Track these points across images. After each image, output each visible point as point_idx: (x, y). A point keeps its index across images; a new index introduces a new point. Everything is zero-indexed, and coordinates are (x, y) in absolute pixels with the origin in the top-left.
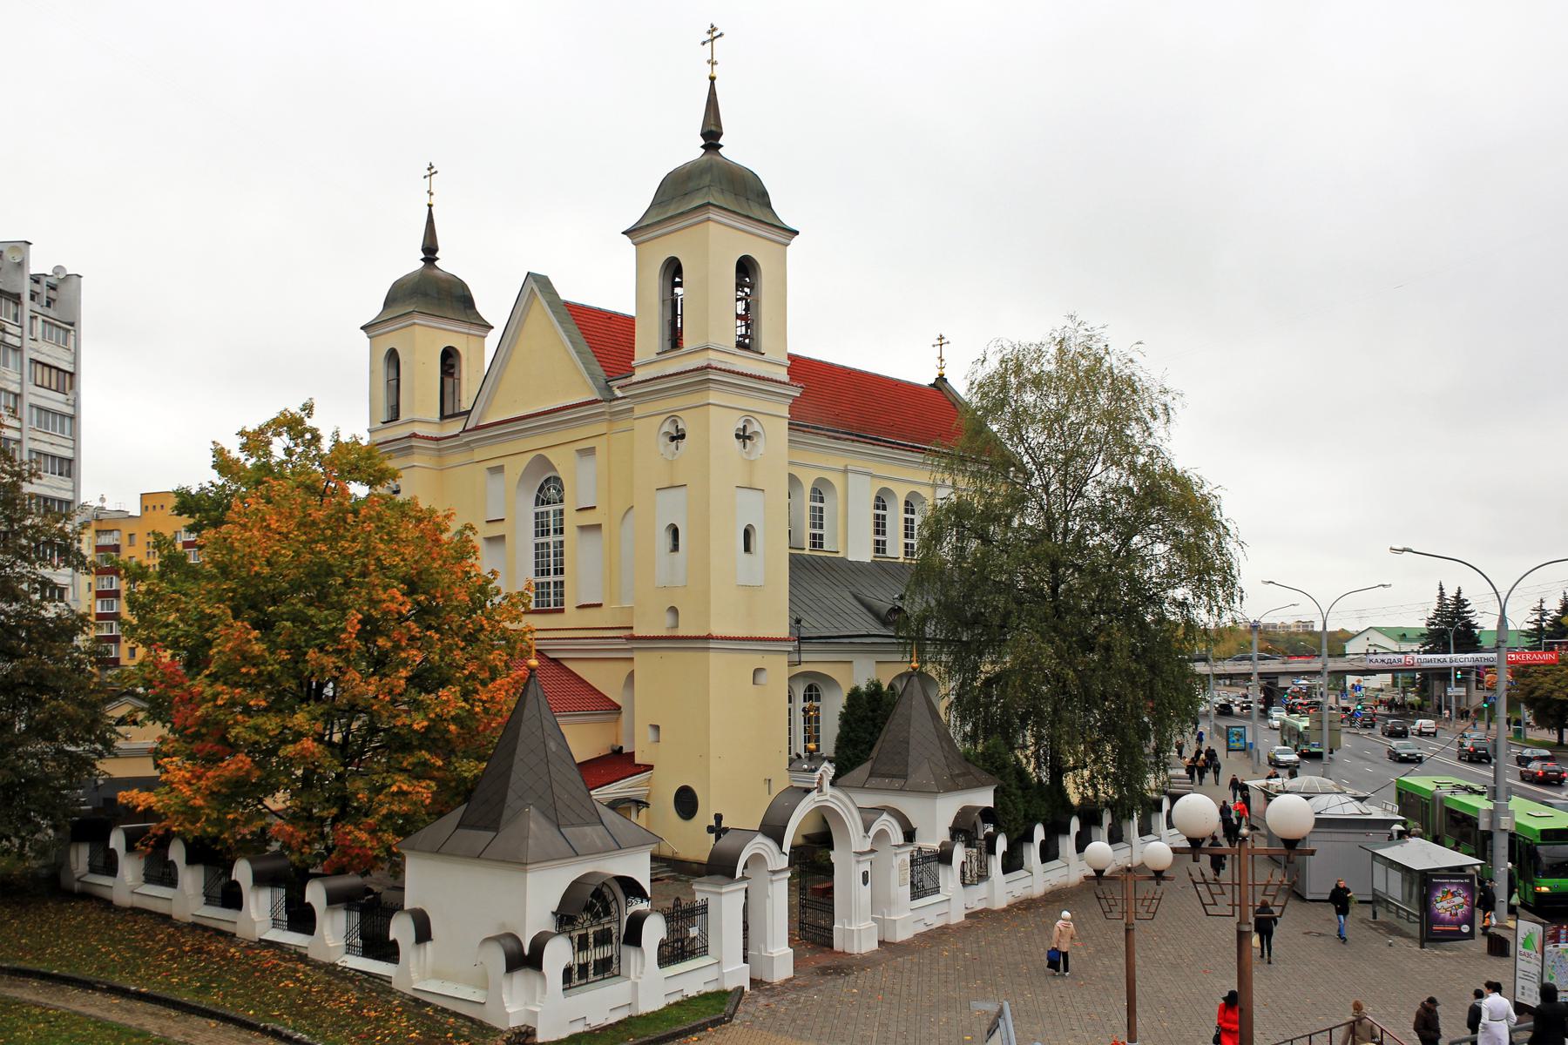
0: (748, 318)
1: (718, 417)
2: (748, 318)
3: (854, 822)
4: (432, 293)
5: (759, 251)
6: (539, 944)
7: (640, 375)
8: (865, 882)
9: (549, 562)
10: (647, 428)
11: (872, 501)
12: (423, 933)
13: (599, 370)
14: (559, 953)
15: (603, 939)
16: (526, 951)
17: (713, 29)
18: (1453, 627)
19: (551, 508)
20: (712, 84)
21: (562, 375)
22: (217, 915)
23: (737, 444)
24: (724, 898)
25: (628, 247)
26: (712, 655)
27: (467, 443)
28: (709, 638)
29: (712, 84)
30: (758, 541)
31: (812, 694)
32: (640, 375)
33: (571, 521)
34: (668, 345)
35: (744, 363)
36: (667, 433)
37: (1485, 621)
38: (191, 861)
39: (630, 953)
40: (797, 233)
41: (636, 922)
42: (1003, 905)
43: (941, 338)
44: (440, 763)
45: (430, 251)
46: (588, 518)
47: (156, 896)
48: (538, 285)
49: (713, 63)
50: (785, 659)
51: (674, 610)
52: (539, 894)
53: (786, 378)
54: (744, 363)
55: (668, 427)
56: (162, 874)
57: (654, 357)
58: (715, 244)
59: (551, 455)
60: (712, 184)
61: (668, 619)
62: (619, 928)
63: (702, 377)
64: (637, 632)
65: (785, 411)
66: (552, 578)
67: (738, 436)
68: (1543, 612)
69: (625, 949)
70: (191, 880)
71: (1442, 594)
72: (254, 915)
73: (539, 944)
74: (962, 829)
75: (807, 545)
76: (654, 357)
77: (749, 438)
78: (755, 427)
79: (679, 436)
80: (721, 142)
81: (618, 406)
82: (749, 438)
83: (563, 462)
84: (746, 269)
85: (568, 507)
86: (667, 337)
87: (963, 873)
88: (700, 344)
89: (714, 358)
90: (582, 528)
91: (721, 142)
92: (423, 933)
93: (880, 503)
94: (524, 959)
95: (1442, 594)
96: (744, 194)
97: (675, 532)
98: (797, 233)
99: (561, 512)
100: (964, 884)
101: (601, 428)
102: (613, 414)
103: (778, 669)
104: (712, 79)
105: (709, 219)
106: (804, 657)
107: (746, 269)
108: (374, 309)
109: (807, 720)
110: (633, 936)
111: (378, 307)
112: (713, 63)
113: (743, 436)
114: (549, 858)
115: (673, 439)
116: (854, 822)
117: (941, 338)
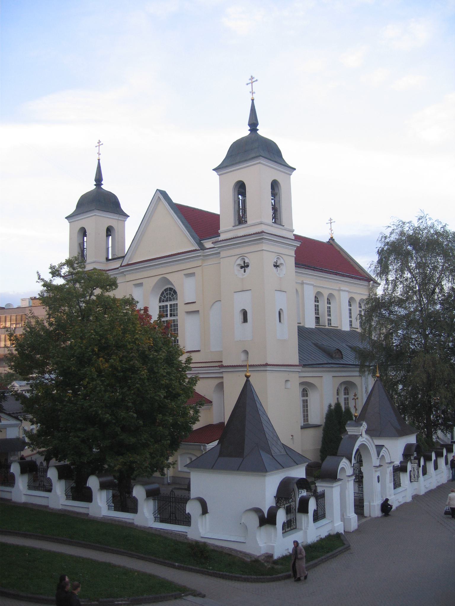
0: (275, 210)
1: (263, 257)
2: (275, 210)
4: (100, 201)
7: (222, 237)
8: (379, 482)
10: (229, 262)
11: (313, 299)
12: (205, 511)
13: (196, 236)
14: (281, 516)
16: (266, 516)
19: (168, 303)
20: (99, 163)
21: (181, 239)
22: (78, 506)
23: (274, 268)
24: (334, 489)
25: (215, 176)
26: (268, 374)
27: (123, 272)
28: (267, 365)
29: (99, 163)
30: (240, 317)
33: (181, 309)
34: (237, 223)
36: (239, 264)
39: (301, 517)
40: (295, 169)
42: (424, 493)
43: (331, 220)
45: (99, 180)
47: (38, 498)
49: (253, 93)
50: (297, 375)
51: (246, 352)
57: (231, 228)
58: (257, 175)
59: (169, 277)
60: (254, 148)
61: (243, 356)
62: (296, 504)
63: (259, 237)
64: (224, 364)
65: (293, 253)
67: (274, 266)
69: (299, 516)
70: (59, 488)
72: (100, 504)
74: (407, 455)
75: (327, 325)
76: (231, 228)
77: (278, 266)
79: (245, 266)
80: (258, 128)
81: (207, 252)
82: (278, 266)
83: (178, 281)
84: (275, 185)
85: (180, 302)
86: (237, 219)
90: (188, 313)
91: (258, 128)
92: (205, 511)
94: (267, 520)
96: (270, 151)
97: (245, 314)
98: (295, 169)
100: (411, 482)
101: (199, 263)
103: (295, 379)
104: (253, 100)
105: (260, 163)
107: (275, 185)
108: (72, 208)
110: (303, 508)
111: (74, 208)
112: (253, 93)
113: (276, 266)
115: (242, 267)
116: (373, 451)
117: (331, 220)
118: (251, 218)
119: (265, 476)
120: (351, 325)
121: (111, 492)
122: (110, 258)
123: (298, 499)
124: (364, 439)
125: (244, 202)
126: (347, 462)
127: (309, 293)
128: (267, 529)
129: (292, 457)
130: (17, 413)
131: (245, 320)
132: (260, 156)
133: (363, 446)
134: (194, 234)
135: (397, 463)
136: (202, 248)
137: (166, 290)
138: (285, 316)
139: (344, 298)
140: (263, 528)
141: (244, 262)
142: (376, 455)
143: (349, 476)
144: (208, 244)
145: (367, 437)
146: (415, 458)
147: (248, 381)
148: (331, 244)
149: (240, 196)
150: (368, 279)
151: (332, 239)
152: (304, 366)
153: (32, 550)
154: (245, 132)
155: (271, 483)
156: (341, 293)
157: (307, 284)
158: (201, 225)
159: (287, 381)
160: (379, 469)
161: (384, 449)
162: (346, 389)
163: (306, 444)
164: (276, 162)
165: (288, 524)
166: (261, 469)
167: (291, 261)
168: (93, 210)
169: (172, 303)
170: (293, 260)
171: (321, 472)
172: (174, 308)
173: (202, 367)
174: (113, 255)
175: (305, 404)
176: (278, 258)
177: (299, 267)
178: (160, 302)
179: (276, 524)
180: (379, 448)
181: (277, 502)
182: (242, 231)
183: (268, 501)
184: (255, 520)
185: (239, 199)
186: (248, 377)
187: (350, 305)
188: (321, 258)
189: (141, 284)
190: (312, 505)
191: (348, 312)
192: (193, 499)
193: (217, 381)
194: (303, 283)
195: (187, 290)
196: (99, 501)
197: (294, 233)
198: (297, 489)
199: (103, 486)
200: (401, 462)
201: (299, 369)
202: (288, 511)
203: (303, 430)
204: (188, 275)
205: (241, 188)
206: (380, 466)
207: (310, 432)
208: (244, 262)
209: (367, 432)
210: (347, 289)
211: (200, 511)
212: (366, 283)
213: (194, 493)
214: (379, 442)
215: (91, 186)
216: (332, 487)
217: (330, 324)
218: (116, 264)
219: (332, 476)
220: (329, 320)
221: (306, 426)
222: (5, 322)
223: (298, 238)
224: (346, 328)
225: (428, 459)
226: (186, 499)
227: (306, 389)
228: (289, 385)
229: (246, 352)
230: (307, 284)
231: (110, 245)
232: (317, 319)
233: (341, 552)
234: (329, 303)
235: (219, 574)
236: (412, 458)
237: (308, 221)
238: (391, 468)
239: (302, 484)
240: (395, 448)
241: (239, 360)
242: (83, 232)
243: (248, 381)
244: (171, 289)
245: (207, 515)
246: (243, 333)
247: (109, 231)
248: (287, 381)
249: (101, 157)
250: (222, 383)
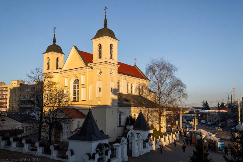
3: (136, 135)
6: (94, 154)
8: (137, 145)
9: (76, 93)
11: (126, 85)
12: (72, 154)
14: (97, 156)
15: (102, 154)
16: (92, 156)
17: (106, 7)
18: (206, 106)
19: (77, 85)
22: (32, 152)
29: (106, 19)
31: (120, 115)
34: (99, 58)
35: (111, 61)
37: (210, 106)
38: (27, 143)
41: (107, 151)
43: (135, 59)
45: (54, 41)
46: (84, 86)
49: (55, 32)
53: (117, 64)
54: (111, 61)
56: (21, 145)
62: (104, 152)
64: (93, 105)
66: (76, 96)
68: (219, 104)
73: (94, 154)
79: (101, 73)
87: (150, 144)
89: (107, 60)
91: (107, 25)
92: (72, 154)
99: (78, 85)
100: (150, 146)
106: (120, 109)
111: (46, 51)
112: (55, 32)
113: (111, 73)
116: (136, 135)
117: (135, 59)
123: (105, 151)
124: (132, 131)
126: (125, 138)
136: (87, 66)
137: (76, 80)
143: (125, 143)
144: (89, 64)
145: (133, 130)
152: (119, 106)
154: (103, 27)
155: (94, 145)
166: (91, 140)
172: (78, 86)
175: (120, 119)
178: (74, 84)
182: (100, 60)
183: (93, 151)
184: (87, 157)
190: (110, 152)
196: (39, 151)
198: (105, 147)
201: (118, 107)
203: (118, 127)
207: (120, 128)
213: (69, 149)
214: (138, 132)
217: (76, 99)
221: (120, 126)
222: (28, 89)
226: (66, 150)
244: (77, 80)
245: (73, 156)
248: (113, 111)
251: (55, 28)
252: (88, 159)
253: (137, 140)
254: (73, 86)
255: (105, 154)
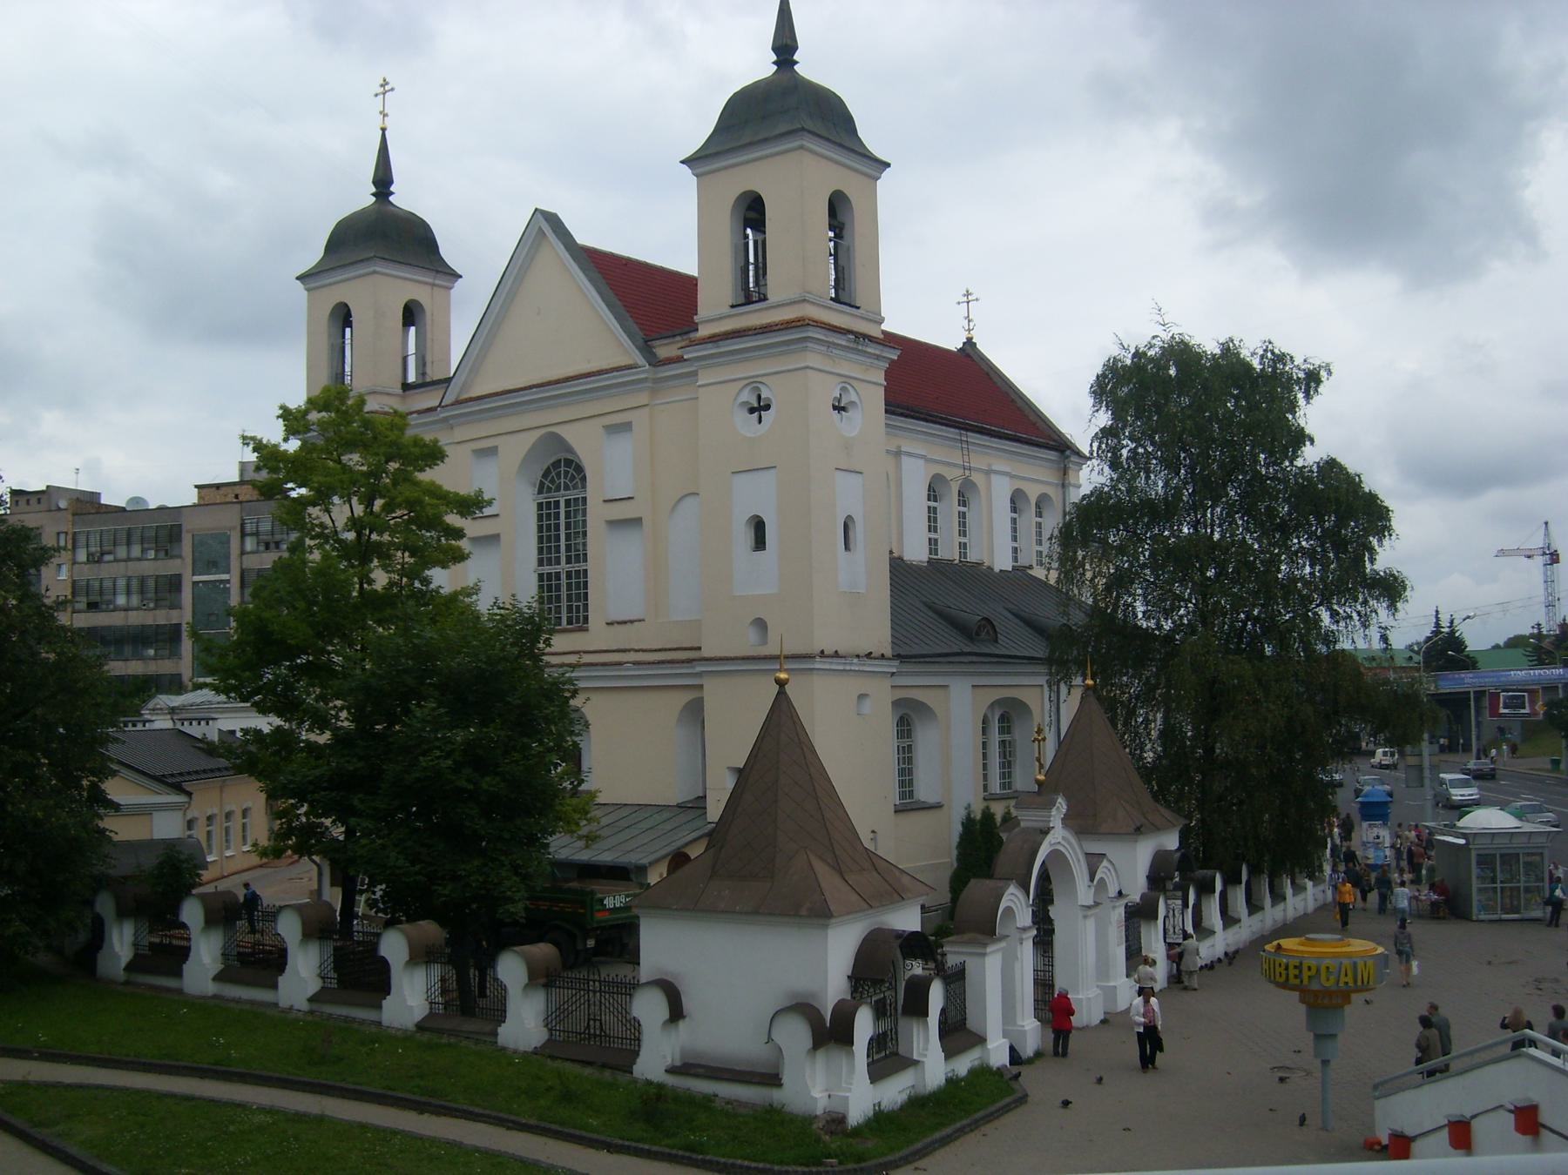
4: (384, 237)
5: (850, 185)
7: (704, 331)
10: (716, 393)
12: (676, 1013)
14: (864, 1025)
20: (384, 135)
21: (592, 335)
27: (445, 420)
29: (384, 135)
31: (1006, 723)
32: (704, 331)
33: (596, 514)
36: (744, 404)
40: (888, 165)
43: (968, 294)
44: (1149, 756)
48: (547, 225)
50: (887, 683)
51: (761, 624)
52: (831, 959)
55: (749, 397)
57: (727, 310)
58: (794, 181)
59: (569, 434)
60: (784, 114)
61: (753, 635)
64: (705, 653)
65: (880, 377)
67: (835, 408)
69: (903, 1023)
71: (1438, 619)
74: (1157, 879)
78: (854, 397)
79: (760, 408)
80: (796, 57)
82: (844, 409)
83: (584, 441)
84: (837, 208)
85: (594, 494)
88: (793, 294)
90: (614, 524)
91: (796, 57)
93: (933, 494)
94: (832, 1033)
95: (1438, 619)
97: (759, 526)
98: (888, 165)
101: (643, 398)
102: (656, 381)
103: (882, 695)
104: (384, 130)
105: (801, 147)
107: (837, 208)
108: (313, 254)
109: (1003, 755)
110: (916, 1006)
113: (839, 408)
114: (850, 912)
115: (752, 410)
116: (1080, 871)
117: (968, 294)
118: (778, 285)
119: (826, 926)
120: (1015, 559)
121: (329, 948)
122: (412, 378)
125: (761, 247)
126: (1020, 894)
127: (915, 478)
128: (836, 1055)
129: (889, 885)
130: (181, 774)
131: (760, 543)
132: (803, 129)
133: (1056, 855)
134: (630, 322)
135: (1135, 897)
137: (556, 464)
138: (858, 533)
139: (1001, 490)
140: (821, 1055)
141: (759, 397)
142: (1087, 877)
144: (664, 350)
146: (1177, 887)
147: (782, 694)
148: (968, 356)
149: (749, 231)
150: (1060, 447)
151: (969, 342)
153: (386, 1135)
154: (762, 66)
156: (994, 477)
157: (910, 454)
158: (647, 300)
159: (862, 697)
160: (1096, 910)
161: (1105, 863)
162: (1004, 718)
163: (922, 848)
164: (841, 145)
165: (879, 1044)
166: (816, 912)
167: (877, 397)
168: (368, 259)
169: (572, 494)
170: (880, 394)
171: (961, 919)
173: (662, 662)
174: (422, 372)
176: (844, 389)
177: (893, 413)
179: (852, 1043)
180: (1094, 861)
181: (854, 990)
182: (754, 317)
183: (834, 985)
185: (746, 237)
186: (781, 684)
187: (1014, 510)
188: (951, 393)
189: (492, 452)
190: (936, 996)
191: (1009, 525)
192: (648, 983)
193: (687, 697)
194: (898, 454)
195: (612, 468)
197: (884, 327)
199: (421, 955)
200: (1143, 896)
202: (880, 1011)
203: (902, 816)
204: (613, 429)
205: (752, 211)
206: (1097, 904)
208: (759, 397)
209: (1067, 820)
210: (1008, 469)
211: (666, 1014)
212: (1052, 455)
213: (646, 971)
214: (1095, 847)
215: (363, 197)
216: (984, 955)
217: (963, 554)
218: (430, 399)
219: (985, 929)
220: (963, 546)
222: (129, 543)
223: (891, 340)
224: (1002, 562)
225: (1205, 888)
226: (629, 988)
227: (907, 718)
228: (867, 706)
229: (761, 624)
230: (910, 454)
231: (412, 349)
232: (933, 543)
233: (1006, 1109)
234: (963, 503)
235: (718, 1163)
236: (1170, 886)
237: (918, 303)
238: (1122, 910)
239: (914, 945)
240: (1132, 863)
241: (747, 643)
242: (343, 317)
243: (782, 694)
244: (569, 462)
245: (682, 1024)
246: (755, 576)
247: (411, 314)
248: (862, 697)
249: (388, 122)
250: (701, 699)
251: (385, 83)
252: (809, 1043)
253: (1089, 907)
254: (534, 508)
255: (904, 1007)
